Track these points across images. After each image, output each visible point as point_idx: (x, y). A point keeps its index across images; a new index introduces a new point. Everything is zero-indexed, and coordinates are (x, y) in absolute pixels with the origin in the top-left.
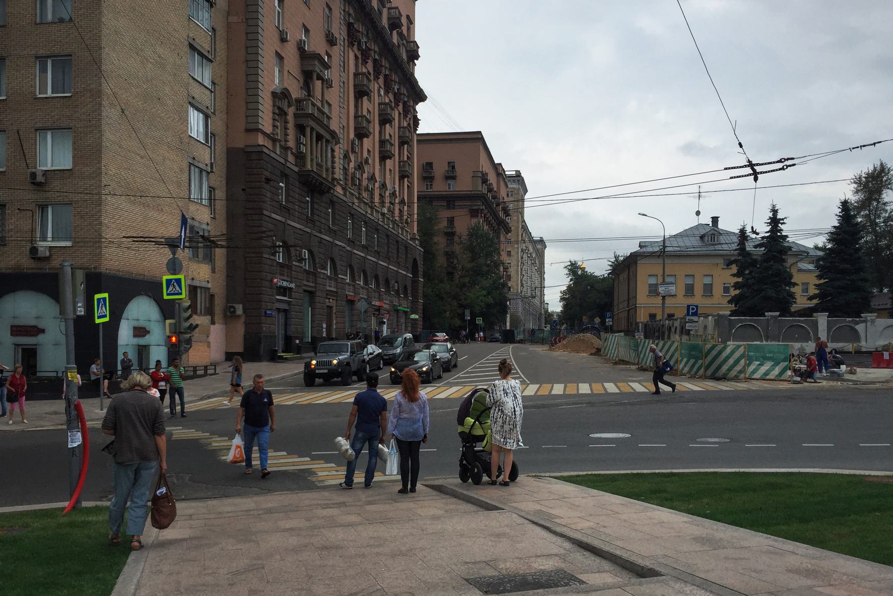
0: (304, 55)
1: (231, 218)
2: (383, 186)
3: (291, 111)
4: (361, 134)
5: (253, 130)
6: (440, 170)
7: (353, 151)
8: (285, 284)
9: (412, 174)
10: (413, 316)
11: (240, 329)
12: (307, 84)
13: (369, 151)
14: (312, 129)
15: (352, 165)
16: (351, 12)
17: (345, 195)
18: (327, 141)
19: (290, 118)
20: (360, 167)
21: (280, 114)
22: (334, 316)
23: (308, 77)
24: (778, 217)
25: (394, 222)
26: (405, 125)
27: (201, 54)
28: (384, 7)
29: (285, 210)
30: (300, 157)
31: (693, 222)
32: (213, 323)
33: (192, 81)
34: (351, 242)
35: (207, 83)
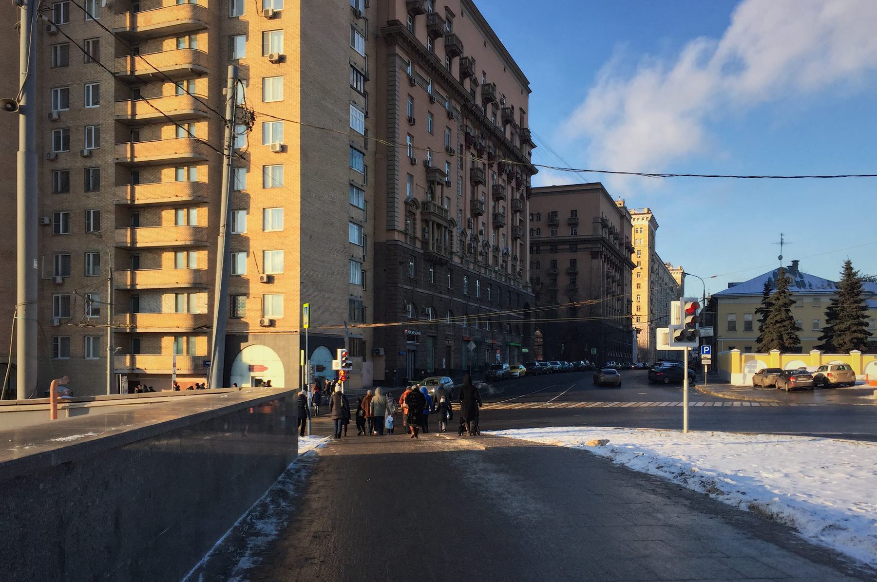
0: (429, 170)
1: (377, 290)
2: (496, 249)
3: (418, 213)
4: (476, 214)
5: (391, 229)
6: (563, 217)
7: (469, 227)
8: (413, 333)
9: (524, 235)
10: (525, 350)
11: (382, 363)
12: (432, 191)
13: (483, 224)
14: (433, 222)
15: (468, 238)
16: (469, 124)
17: (462, 263)
18: (446, 227)
19: (418, 217)
20: (475, 238)
21: (410, 214)
22: (453, 354)
23: (431, 184)
24: (383, 378)
25: (507, 275)
26: (518, 197)
27: (358, 189)
28: (498, 109)
29: (414, 282)
30: (425, 243)
31: (775, 265)
32: (364, 360)
33: (352, 207)
34: (468, 298)
35: (361, 206)
